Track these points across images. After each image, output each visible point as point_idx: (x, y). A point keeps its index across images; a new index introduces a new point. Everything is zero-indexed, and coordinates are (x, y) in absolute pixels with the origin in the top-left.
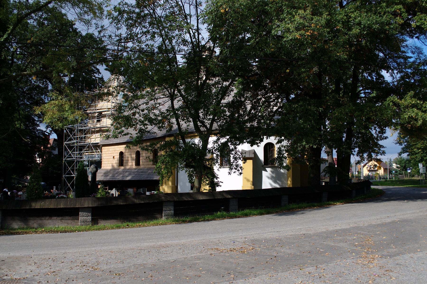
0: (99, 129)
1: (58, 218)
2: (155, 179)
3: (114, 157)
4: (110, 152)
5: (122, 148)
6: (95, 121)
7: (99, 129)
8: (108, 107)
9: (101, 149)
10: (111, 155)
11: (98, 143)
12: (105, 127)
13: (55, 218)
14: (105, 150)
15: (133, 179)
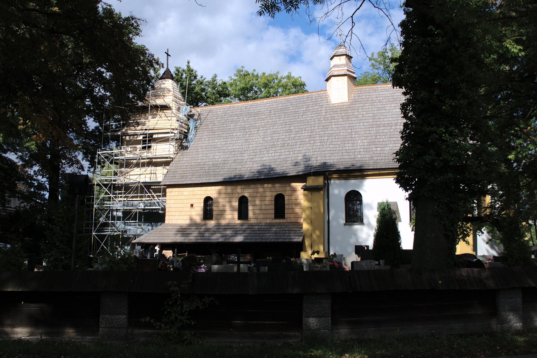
2: (295, 240)
3: (192, 205)
4: (183, 197)
5: (212, 192)
7: (148, 160)
8: (172, 127)
11: (160, 182)
12: (167, 158)
14: (173, 194)
15: (248, 241)
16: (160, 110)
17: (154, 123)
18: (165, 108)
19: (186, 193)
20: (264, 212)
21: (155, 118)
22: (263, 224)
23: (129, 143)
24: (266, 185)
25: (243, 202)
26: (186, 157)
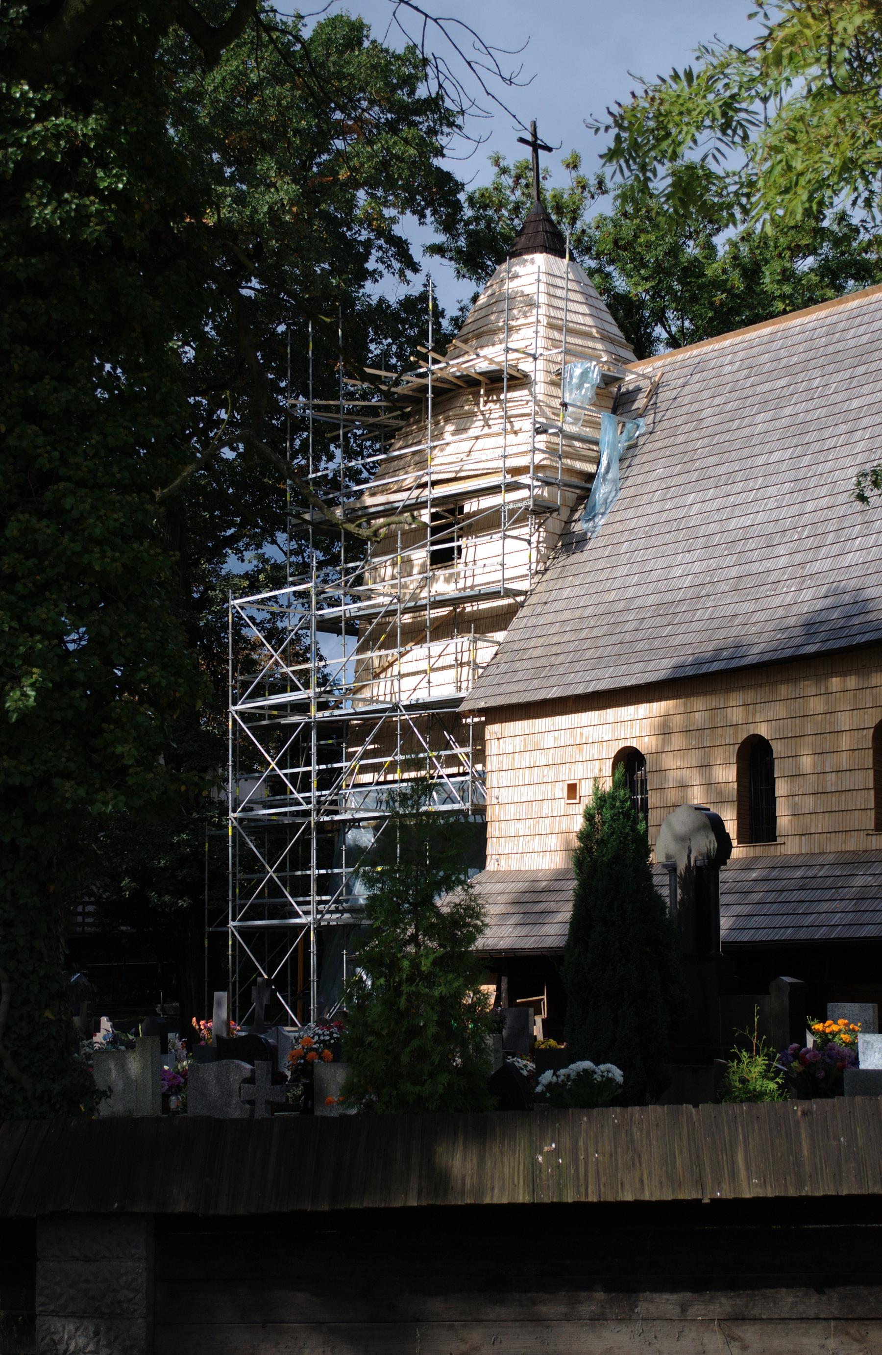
0: (443, 611)
1: (697, 1310)
4: (541, 759)
6: (420, 556)
7: (443, 611)
8: (512, 463)
9: (480, 739)
10: (550, 774)
12: (495, 595)
13: (667, 1303)
14: (508, 746)
15: (746, 937)
16: (488, 393)
17: (474, 452)
18: (497, 382)
19: (549, 741)
20: (834, 802)
21: (465, 430)
22: (830, 859)
23: (387, 546)
24: (835, 683)
25: (756, 759)
26: (583, 583)
